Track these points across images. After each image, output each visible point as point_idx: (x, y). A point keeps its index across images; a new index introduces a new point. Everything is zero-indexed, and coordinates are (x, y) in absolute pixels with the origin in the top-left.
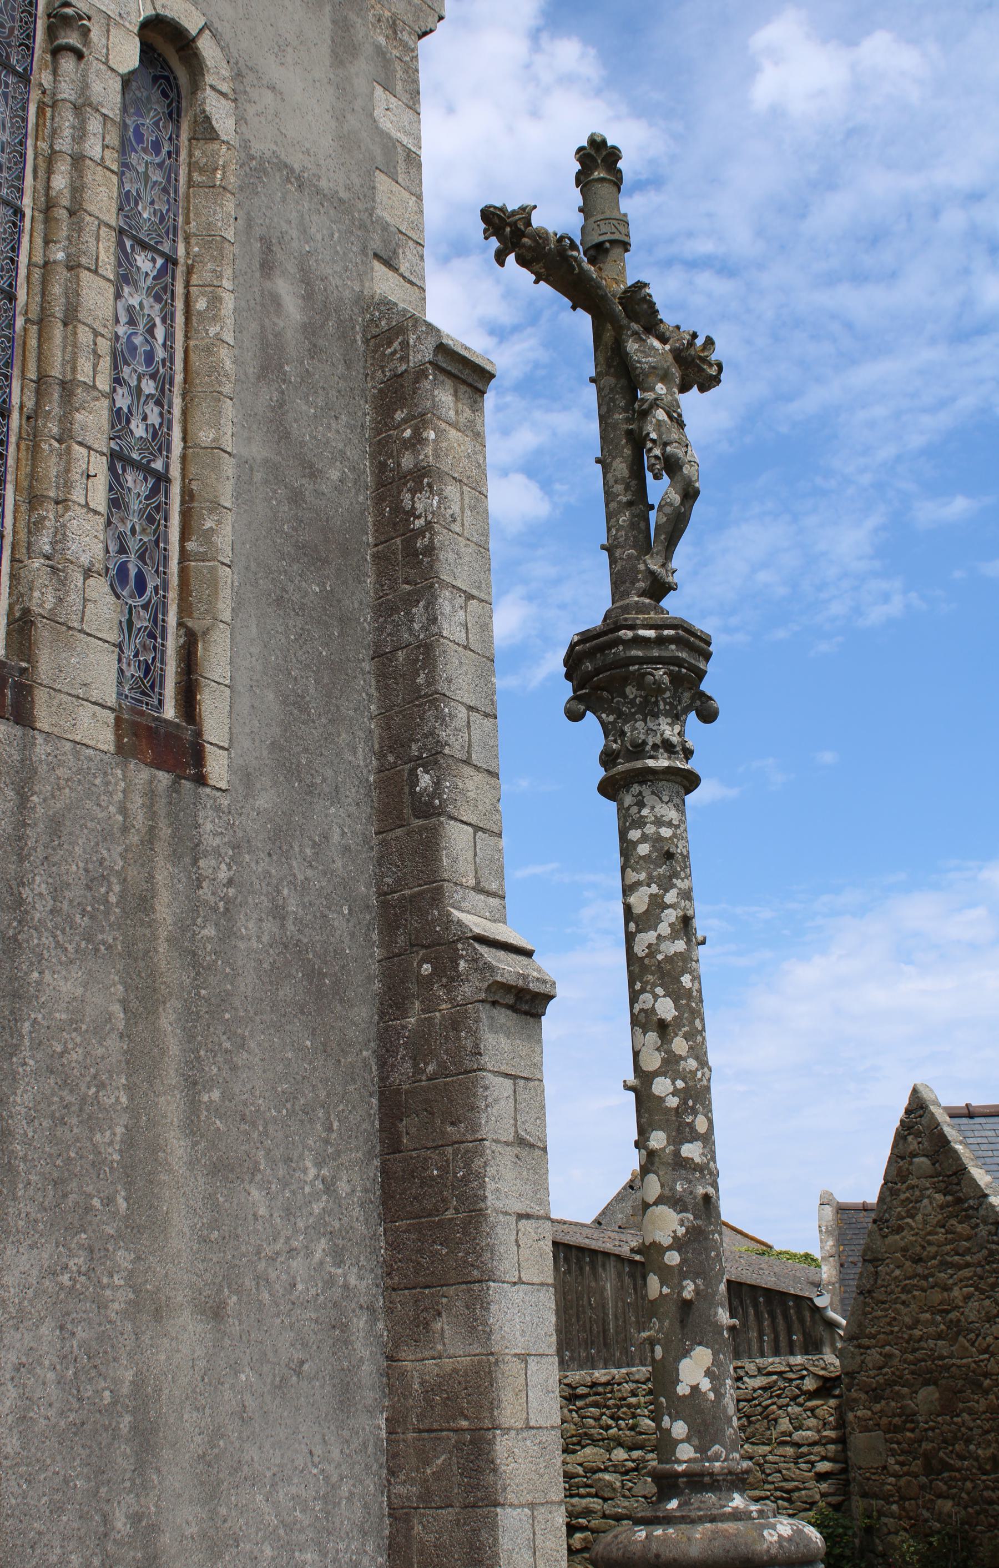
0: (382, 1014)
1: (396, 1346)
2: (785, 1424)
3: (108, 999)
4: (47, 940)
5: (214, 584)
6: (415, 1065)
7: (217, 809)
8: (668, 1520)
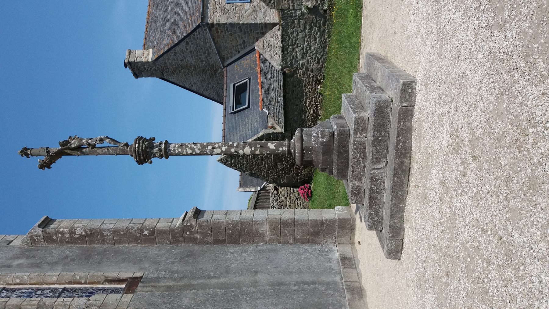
0: (197, 244)
1: (264, 241)
2: (283, 198)
3: (190, 293)
4: (176, 305)
5: (94, 276)
6: (208, 236)
7: (148, 274)
8: (295, 151)
